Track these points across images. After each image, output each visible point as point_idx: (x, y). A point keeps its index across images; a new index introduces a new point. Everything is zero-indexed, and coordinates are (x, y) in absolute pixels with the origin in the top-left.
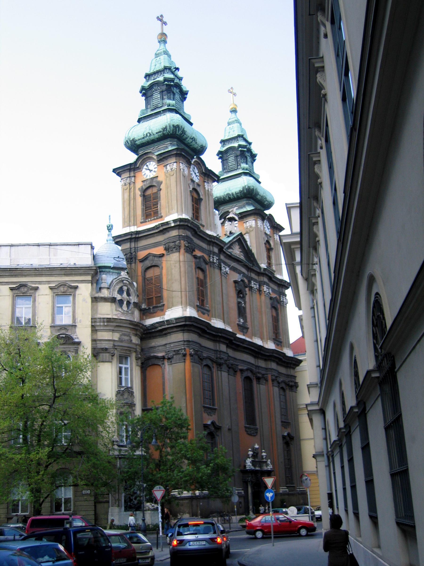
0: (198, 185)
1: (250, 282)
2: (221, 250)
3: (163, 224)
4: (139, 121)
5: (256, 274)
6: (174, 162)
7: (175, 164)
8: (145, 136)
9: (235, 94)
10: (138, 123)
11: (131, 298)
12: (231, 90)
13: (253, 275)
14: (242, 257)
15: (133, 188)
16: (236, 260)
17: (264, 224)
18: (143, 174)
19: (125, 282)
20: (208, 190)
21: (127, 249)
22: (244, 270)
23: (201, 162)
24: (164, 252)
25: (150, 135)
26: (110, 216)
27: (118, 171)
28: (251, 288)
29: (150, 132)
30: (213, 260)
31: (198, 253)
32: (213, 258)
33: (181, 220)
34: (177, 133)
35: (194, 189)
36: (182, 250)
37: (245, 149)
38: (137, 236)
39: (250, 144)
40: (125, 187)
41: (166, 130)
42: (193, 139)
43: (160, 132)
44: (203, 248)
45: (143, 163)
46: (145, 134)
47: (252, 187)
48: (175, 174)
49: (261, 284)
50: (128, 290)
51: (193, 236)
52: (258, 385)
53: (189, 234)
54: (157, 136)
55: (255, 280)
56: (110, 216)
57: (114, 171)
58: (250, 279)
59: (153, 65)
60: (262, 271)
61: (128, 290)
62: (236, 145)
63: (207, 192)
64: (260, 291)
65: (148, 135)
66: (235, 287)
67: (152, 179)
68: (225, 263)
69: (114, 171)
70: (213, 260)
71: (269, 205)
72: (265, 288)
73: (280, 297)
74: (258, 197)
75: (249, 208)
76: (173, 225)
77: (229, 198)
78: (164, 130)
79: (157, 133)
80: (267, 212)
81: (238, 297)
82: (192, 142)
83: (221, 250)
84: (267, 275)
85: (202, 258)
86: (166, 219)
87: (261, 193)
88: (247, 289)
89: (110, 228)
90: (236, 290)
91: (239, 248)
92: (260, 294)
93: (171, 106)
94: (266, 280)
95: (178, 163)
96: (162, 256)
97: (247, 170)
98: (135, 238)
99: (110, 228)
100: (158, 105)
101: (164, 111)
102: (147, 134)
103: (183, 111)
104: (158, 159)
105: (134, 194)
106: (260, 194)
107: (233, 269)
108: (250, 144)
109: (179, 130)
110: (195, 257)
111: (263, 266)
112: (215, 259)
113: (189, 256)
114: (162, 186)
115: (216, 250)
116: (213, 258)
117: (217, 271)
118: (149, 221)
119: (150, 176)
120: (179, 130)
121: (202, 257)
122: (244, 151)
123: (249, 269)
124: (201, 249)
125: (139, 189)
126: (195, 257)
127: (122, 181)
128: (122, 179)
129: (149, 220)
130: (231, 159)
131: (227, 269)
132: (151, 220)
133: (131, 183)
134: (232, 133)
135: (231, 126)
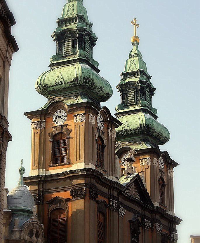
0: (103, 133)
1: (143, 220)
2: (120, 193)
3: (71, 172)
4: (51, 66)
5: (149, 212)
6: (83, 114)
7: (84, 115)
8: (57, 84)
9: (137, 26)
10: (49, 69)
11: (39, 239)
12: (134, 21)
13: (147, 214)
14: (137, 197)
15: (43, 133)
16: (133, 201)
17: (159, 161)
18: (54, 120)
19: (35, 225)
20: (111, 137)
21: (35, 190)
22: (138, 209)
23: (106, 111)
24: (71, 197)
25: (62, 83)
26: (22, 160)
27: (31, 115)
28: (144, 227)
29: (62, 80)
30: (113, 204)
31: (100, 198)
32: (113, 201)
33: (88, 170)
34: (87, 84)
35: (100, 137)
36: (88, 197)
37: (145, 85)
38: (46, 179)
39: (150, 78)
40: (36, 131)
41: (77, 81)
42: (101, 89)
43: (71, 82)
44: (104, 192)
45: (54, 110)
46: (57, 82)
47: (150, 126)
48: (84, 125)
49: (154, 221)
50: (37, 232)
51: (97, 182)
52: (110, 93)
53: (93, 181)
54: (68, 85)
55: (148, 219)
56: (22, 160)
57: (26, 114)
58: (143, 217)
59: (66, 10)
60: (155, 209)
61: (37, 232)
62: (136, 79)
63: (110, 138)
64: (152, 228)
65: (60, 83)
66: (130, 227)
67: (62, 126)
68: (123, 205)
69: (26, 114)
70: (113, 204)
71: (164, 140)
72: (157, 226)
73: (170, 233)
74: (155, 134)
75: (146, 146)
76: (80, 174)
77: (127, 133)
78: (75, 81)
79: (68, 83)
80: (162, 148)
81: (133, 236)
82: (99, 91)
83: (120, 193)
84: (159, 213)
85: (104, 203)
86: (74, 167)
87: (158, 130)
88: (140, 228)
89: (22, 171)
90: (131, 229)
91: (135, 188)
92: (152, 232)
93: (82, 56)
94: (158, 217)
95: (87, 115)
96: (68, 200)
97: (145, 106)
98: (43, 181)
99: (22, 171)
100: (69, 52)
101: (75, 61)
102: (58, 83)
103: (92, 57)
104: (69, 109)
105: (45, 138)
106: (156, 131)
107: (128, 209)
108: (150, 78)
109: (89, 82)
110: (97, 202)
111: (157, 204)
112: (114, 203)
113: (93, 202)
114: (72, 135)
115: (115, 194)
116: (113, 201)
117: (115, 213)
118: (57, 166)
119: (60, 123)
120: (89, 82)
121: (104, 202)
122: (144, 87)
123: (143, 208)
124: (103, 194)
125: (49, 134)
126: (97, 202)
127: (33, 124)
128: (33, 123)
129: (58, 165)
130: (131, 95)
131: (124, 210)
132: (59, 166)
133: (42, 128)
134: (133, 66)
135: (132, 59)
